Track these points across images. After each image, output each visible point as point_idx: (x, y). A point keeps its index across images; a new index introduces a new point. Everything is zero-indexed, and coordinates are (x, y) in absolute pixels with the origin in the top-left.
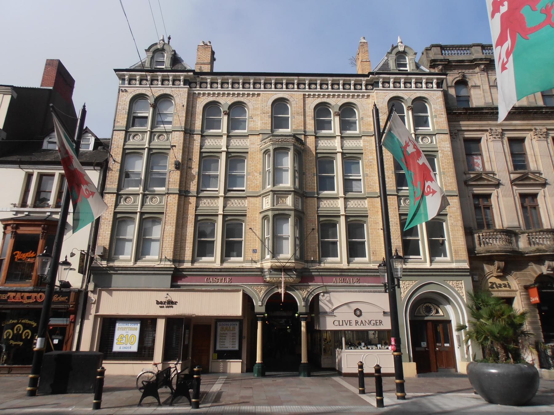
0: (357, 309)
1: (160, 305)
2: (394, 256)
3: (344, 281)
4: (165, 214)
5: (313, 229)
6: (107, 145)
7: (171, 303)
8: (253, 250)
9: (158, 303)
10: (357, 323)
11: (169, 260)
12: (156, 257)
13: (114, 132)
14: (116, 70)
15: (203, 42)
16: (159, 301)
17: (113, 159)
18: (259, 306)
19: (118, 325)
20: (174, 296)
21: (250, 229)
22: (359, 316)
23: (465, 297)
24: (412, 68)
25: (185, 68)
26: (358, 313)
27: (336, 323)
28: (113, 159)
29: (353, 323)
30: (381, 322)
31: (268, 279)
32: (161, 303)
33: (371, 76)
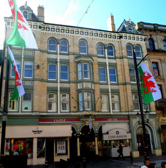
0: (117, 131)
1: (34, 133)
2: (91, 130)
4: (152, 68)
5: (98, 98)
6: (150, 52)
7: (39, 132)
8: (74, 107)
9: (33, 131)
12: (30, 110)
13: (157, 48)
14: (5, 18)
15: (41, 9)
16: (34, 131)
18: (79, 131)
20: (40, 128)
21: (72, 97)
22: (118, 134)
23: (155, 125)
24: (30, 18)
26: (117, 133)
30: (126, 136)
32: (35, 131)
33: (120, 33)
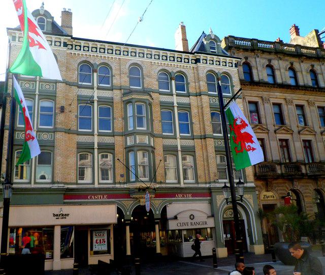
0: (192, 215)
1: (56, 217)
3: (183, 196)
7: (64, 216)
9: (54, 215)
10: (191, 224)
11: (297, 158)
14: (8, 29)
16: (56, 214)
17: (301, 131)
18: (128, 214)
19: (55, 227)
20: (66, 209)
21: (118, 159)
22: (192, 219)
25: (63, 33)
26: (192, 217)
27: (179, 225)
28: (301, 131)
29: (190, 224)
30: (206, 223)
31: (279, 172)
32: (57, 215)
33: (196, 54)
